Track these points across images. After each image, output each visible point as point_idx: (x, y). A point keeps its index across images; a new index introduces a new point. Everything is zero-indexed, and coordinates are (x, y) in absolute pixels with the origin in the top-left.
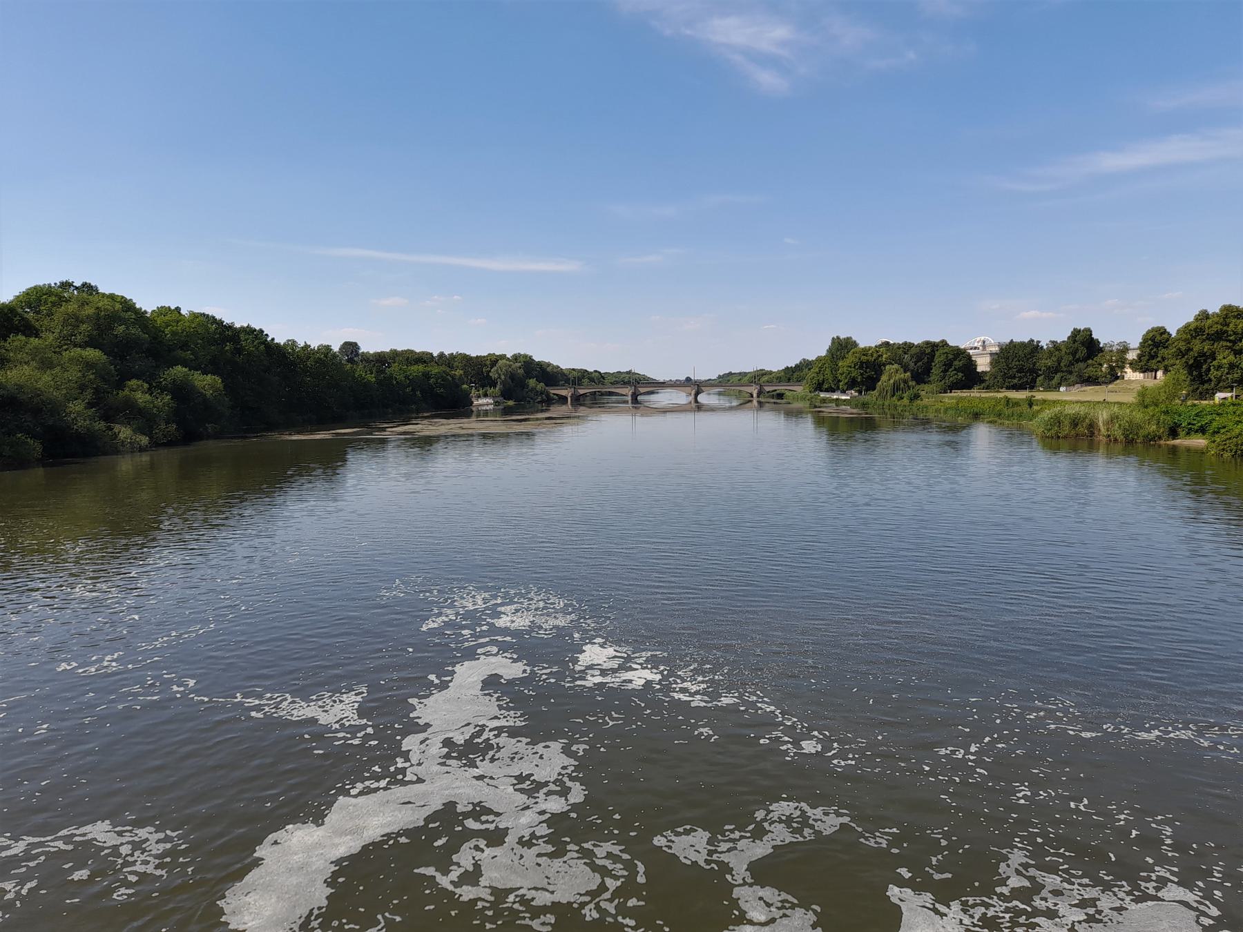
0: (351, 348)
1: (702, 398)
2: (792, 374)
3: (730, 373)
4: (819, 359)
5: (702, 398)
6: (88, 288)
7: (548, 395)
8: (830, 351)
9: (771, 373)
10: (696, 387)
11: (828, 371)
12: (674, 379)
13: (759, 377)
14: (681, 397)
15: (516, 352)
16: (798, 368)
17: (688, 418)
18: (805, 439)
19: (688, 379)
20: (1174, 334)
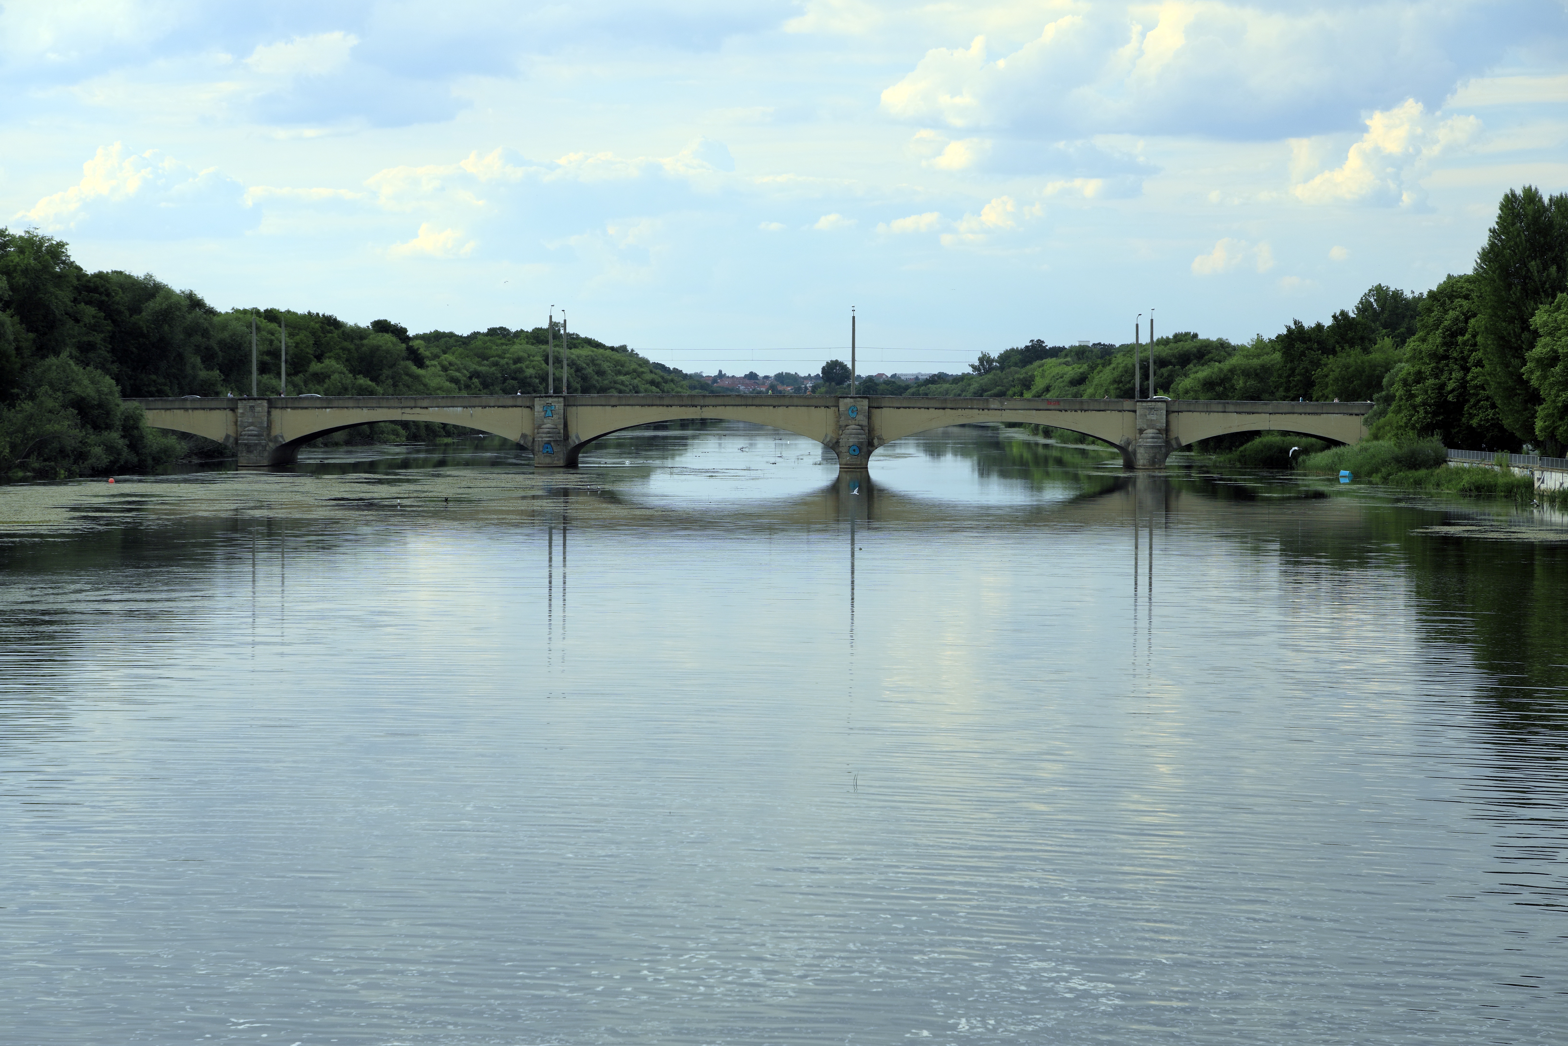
0: (1440, 284)
1: (898, 470)
2: (1303, 361)
3: (1037, 352)
4: (1451, 292)
5: (898, 470)
6: (752, 376)
7: (131, 428)
8: (1490, 255)
9: (1223, 348)
10: (850, 408)
11: (1485, 350)
12: (767, 369)
13: (1175, 366)
14: (797, 468)
15: (1498, 205)
16: (1346, 331)
17: (822, 560)
18: (1336, 671)
19: (836, 373)
20: (1546, 200)
